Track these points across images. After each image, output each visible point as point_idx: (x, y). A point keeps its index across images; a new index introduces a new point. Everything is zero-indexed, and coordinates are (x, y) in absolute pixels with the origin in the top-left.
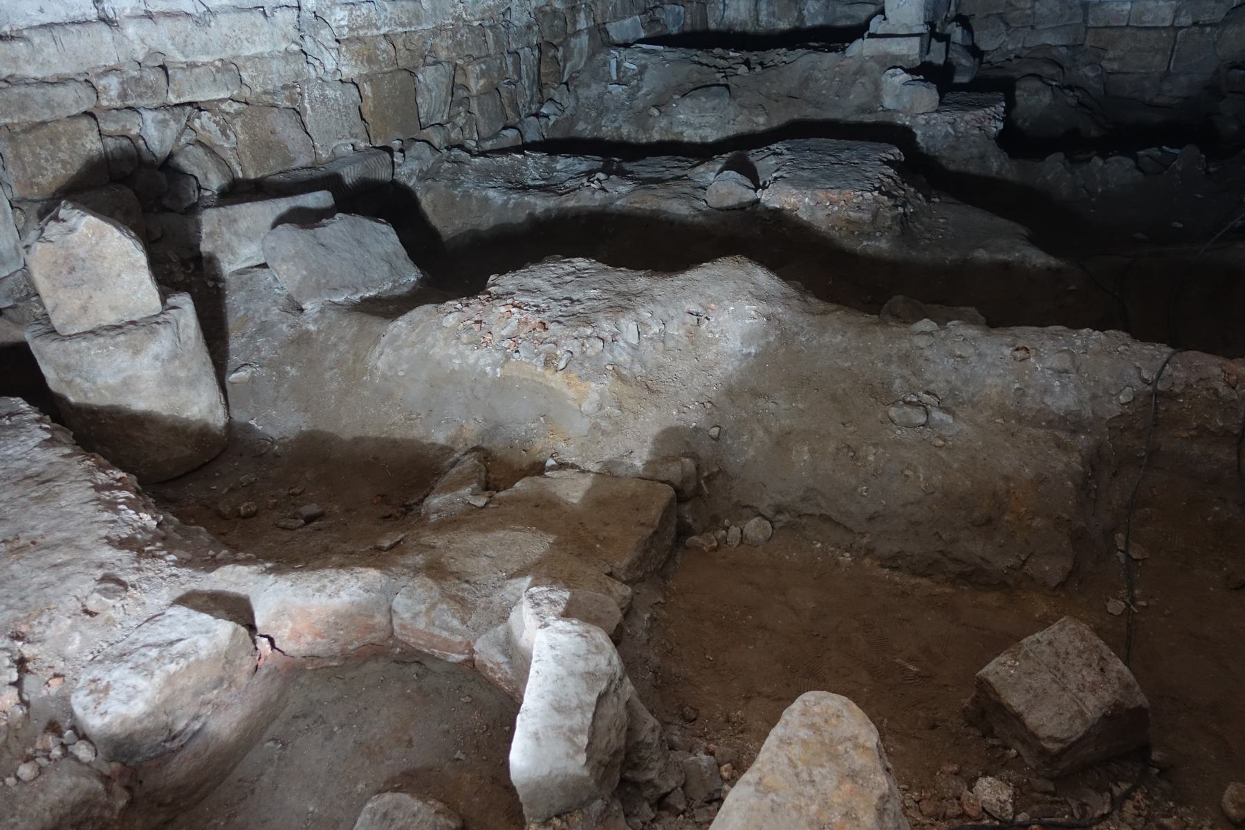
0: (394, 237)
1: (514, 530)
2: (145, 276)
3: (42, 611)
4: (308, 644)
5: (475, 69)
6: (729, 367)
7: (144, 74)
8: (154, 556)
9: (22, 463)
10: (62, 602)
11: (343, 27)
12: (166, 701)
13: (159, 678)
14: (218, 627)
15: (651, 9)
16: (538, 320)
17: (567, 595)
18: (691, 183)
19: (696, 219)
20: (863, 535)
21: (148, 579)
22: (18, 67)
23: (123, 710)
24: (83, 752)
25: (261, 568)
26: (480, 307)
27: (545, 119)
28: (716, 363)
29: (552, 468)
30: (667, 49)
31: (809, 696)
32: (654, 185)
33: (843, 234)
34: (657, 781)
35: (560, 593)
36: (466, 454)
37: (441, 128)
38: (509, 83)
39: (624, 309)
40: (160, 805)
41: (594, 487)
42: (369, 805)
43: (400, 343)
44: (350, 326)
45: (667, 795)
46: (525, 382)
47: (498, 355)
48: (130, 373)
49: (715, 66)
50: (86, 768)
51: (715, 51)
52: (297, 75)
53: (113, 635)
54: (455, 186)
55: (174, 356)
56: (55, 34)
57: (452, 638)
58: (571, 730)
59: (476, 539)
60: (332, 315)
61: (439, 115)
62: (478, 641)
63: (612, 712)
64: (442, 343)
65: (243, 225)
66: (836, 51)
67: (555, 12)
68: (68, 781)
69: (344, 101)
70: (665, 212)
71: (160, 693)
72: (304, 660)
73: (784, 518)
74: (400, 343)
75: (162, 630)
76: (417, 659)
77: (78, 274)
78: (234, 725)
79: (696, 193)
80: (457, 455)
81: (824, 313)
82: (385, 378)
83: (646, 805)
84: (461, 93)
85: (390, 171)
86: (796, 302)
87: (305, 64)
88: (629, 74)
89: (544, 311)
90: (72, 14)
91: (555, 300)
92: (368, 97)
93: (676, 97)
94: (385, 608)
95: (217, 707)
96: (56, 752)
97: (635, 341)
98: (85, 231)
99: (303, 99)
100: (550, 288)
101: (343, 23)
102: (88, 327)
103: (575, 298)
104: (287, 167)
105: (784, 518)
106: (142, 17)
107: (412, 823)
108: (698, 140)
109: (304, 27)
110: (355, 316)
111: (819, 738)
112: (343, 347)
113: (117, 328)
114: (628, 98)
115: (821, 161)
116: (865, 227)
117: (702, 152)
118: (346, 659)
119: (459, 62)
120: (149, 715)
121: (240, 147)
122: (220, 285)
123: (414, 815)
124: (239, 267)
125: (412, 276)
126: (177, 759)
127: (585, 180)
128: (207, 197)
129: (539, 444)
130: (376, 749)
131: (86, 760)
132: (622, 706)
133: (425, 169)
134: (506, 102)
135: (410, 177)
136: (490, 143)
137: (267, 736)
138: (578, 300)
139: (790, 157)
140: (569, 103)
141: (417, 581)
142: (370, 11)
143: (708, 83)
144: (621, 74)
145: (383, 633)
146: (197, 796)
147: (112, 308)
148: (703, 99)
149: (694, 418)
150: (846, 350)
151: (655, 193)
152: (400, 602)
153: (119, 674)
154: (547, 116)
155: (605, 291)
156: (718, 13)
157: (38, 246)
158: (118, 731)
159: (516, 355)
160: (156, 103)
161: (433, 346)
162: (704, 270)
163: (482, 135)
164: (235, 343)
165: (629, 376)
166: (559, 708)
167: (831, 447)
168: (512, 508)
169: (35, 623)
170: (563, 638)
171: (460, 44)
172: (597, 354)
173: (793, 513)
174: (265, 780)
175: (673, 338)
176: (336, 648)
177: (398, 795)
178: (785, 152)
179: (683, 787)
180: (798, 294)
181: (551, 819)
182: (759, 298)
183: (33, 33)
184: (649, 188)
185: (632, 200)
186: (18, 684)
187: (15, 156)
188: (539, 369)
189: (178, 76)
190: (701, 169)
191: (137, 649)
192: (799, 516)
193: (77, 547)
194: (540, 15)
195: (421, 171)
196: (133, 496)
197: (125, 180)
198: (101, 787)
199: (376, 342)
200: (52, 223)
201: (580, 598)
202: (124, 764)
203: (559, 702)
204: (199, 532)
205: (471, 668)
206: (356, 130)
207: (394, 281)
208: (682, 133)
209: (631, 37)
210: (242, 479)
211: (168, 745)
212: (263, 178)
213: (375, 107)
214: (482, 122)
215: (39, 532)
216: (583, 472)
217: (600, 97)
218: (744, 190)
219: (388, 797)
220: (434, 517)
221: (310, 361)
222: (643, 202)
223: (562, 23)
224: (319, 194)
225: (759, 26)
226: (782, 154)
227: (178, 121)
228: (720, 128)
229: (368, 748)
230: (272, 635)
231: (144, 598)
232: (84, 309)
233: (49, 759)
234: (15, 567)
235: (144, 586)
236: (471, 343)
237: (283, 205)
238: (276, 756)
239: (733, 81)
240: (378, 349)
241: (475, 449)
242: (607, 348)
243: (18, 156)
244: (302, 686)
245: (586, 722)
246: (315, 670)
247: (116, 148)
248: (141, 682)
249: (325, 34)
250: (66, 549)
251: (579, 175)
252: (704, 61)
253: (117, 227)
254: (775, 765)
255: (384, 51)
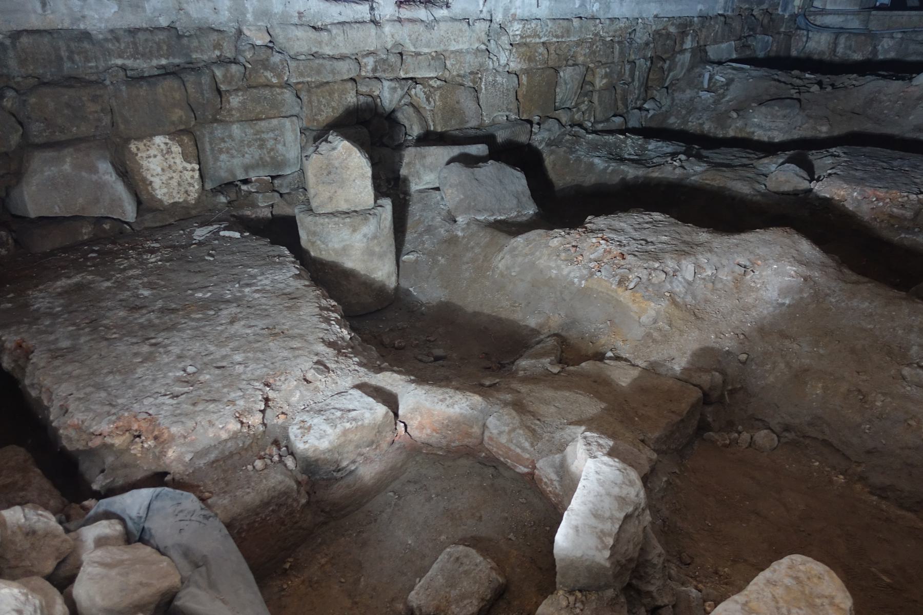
0: (524, 182)
1: (577, 393)
2: (369, 183)
3: (282, 373)
4: (427, 435)
5: (601, 71)
6: (766, 311)
7: (389, 57)
8: (346, 356)
9: (282, 285)
10: (293, 370)
11: (517, 35)
12: (340, 445)
13: (339, 429)
14: (378, 408)
15: (744, 37)
16: (619, 251)
17: (611, 443)
18: (755, 170)
19: (754, 198)
20: (859, 464)
21: (342, 369)
22: (321, 48)
23: (316, 443)
24: (290, 462)
25: (408, 378)
26: (578, 236)
27: (646, 112)
28: (754, 306)
29: (610, 358)
30: (753, 68)
31: (798, 558)
32: (724, 169)
33: (883, 225)
34: (655, 594)
35: (607, 440)
36: (548, 337)
37: (568, 111)
38: (624, 84)
39: (686, 254)
40: (322, 511)
41: (639, 377)
42: (448, 550)
43: (516, 253)
44: (485, 237)
45: (659, 607)
46: (601, 294)
47: (585, 272)
48: (348, 243)
49: (791, 84)
50: (290, 473)
51: (793, 72)
52: (481, 65)
53: (318, 397)
54: (572, 152)
55: (375, 237)
56: (345, 28)
57: (523, 454)
58: (602, 531)
59: (549, 393)
60: (474, 227)
61: (570, 102)
62: (540, 461)
63: (633, 530)
64: (546, 258)
65: (429, 160)
66: (903, 79)
67: (669, 35)
68: (280, 477)
69: (507, 86)
70: (730, 190)
71: (338, 439)
72: (422, 445)
73: (790, 436)
74: (516, 253)
75: (345, 401)
76: (495, 464)
77: (332, 176)
78: (373, 475)
79: (759, 178)
80: (542, 337)
81: (856, 283)
82: (502, 275)
83: (643, 610)
84: (589, 88)
85: (528, 136)
86: (832, 270)
87: (487, 59)
88: (718, 84)
89: (624, 246)
90: (356, 17)
91: (634, 240)
92: (523, 84)
93: (753, 105)
94: (481, 423)
95: (367, 460)
96: (276, 458)
97: (690, 278)
98: (342, 150)
99: (481, 82)
100: (631, 231)
101: (517, 33)
102: (330, 211)
103: (649, 240)
104: (461, 127)
105: (790, 436)
106: (395, 21)
107: (474, 569)
108: (766, 139)
109: (491, 34)
110: (489, 230)
111: (801, 589)
112: (477, 250)
113: (346, 213)
114: (714, 102)
115: (874, 165)
116: (906, 223)
117: (769, 149)
118: (449, 452)
119: (591, 65)
120: (329, 451)
121: (436, 110)
122: (407, 198)
123: (476, 565)
124: (421, 188)
125: (531, 210)
126: (336, 485)
127: (669, 159)
128: (409, 140)
129: (603, 340)
130: (457, 516)
131: (291, 468)
132: (641, 529)
133: (552, 138)
134: (619, 97)
135: (541, 143)
136: (602, 125)
137: (390, 488)
138: (652, 242)
139: (846, 159)
140: (666, 102)
141: (506, 411)
142: (537, 26)
143: (783, 97)
144: (712, 84)
145: (475, 440)
146: (343, 513)
147: (346, 201)
148: (777, 108)
149: (728, 344)
150: (871, 315)
151: (725, 174)
152: (492, 422)
153: (317, 421)
154: (648, 110)
155: (673, 239)
156: (800, 44)
157: (314, 156)
158: (311, 455)
159: (599, 274)
160: (392, 76)
161: (540, 258)
162: (756, 234)
163: (597, 119)
164: (410, 236)
165: (681, 303)
166: (596, 514)
167: (844, 388)
168: (577, 379)
169: (277, 379)
170: (606, 469)
171: (594, 52)
172: (660, 283)
173: (798, 433)
174: (385, 515)
175: (722, 282)
176: (444, 442)
177: (468, 549)
178: (843, 155)
179: (674, 606)
180: (835, 264)
181: (575, 591)
182: (801, 263)
183: (333, 27)
184: (719, 170)
185: (704, 177)
186: (263, 411)
187: (308, 102)
188: (613, 286)
189: (408, 60)
190: (766, 161)
191: (330, 409)
192: (804, 437)
193: (305, 340)
194: (657, 36)
195: (549, 139)
196: (339, 317)
197: (364, 123)
198: (295, 486)
199: (500, 250)
200: (324, 143)
201: (621, 448)
202: (309, 477)
203: (597, 511)
204: (372, 350)
205: (531, 480)
206: (511, 107)
207: (519, 212)
208: (753, 133)
209: (725, 57)
210: (398, 324)
211: (335, 474)
212: (446, 132)
213: (527, 91)
214: (598, 110)
215: (286, 327)
216: (633, 365)
217: (692, 100)
218: (801, 180)
219: (461, 548)
220: (521, 373)
221: (455, 255)
222: (712, 180)
223: (672, 43)
224: (480, 146)
225: (835, 56)
226: (838, 156)
227: (402, 89)
228: (787, 132)
229: (452, 514)
230: (407, 423)
231: (337, 379)
232: (331, 198)
233: (272, 462)
234: (271, 344)
235: (339, 372)
236: (566, 260)
237: (456, 150)
238: (393, 503)
239: (804, 97)
240: (501, 255)
241: (555, 335)
242: (668, 279)
243: (310, 102)
244: (417, 462)
245: (613, 529)
246: (427, 454)
247: (363, 103)
248: (329, 430)
249: (504, 39)
250: (299, 340)
251: (665, 155)
252: (783, 79)
253: (359, 150)
254: (760, 596)
255: (541, 54)
